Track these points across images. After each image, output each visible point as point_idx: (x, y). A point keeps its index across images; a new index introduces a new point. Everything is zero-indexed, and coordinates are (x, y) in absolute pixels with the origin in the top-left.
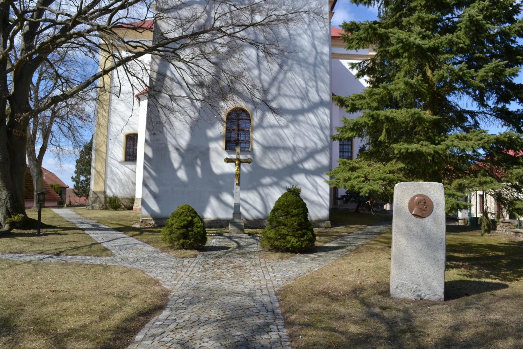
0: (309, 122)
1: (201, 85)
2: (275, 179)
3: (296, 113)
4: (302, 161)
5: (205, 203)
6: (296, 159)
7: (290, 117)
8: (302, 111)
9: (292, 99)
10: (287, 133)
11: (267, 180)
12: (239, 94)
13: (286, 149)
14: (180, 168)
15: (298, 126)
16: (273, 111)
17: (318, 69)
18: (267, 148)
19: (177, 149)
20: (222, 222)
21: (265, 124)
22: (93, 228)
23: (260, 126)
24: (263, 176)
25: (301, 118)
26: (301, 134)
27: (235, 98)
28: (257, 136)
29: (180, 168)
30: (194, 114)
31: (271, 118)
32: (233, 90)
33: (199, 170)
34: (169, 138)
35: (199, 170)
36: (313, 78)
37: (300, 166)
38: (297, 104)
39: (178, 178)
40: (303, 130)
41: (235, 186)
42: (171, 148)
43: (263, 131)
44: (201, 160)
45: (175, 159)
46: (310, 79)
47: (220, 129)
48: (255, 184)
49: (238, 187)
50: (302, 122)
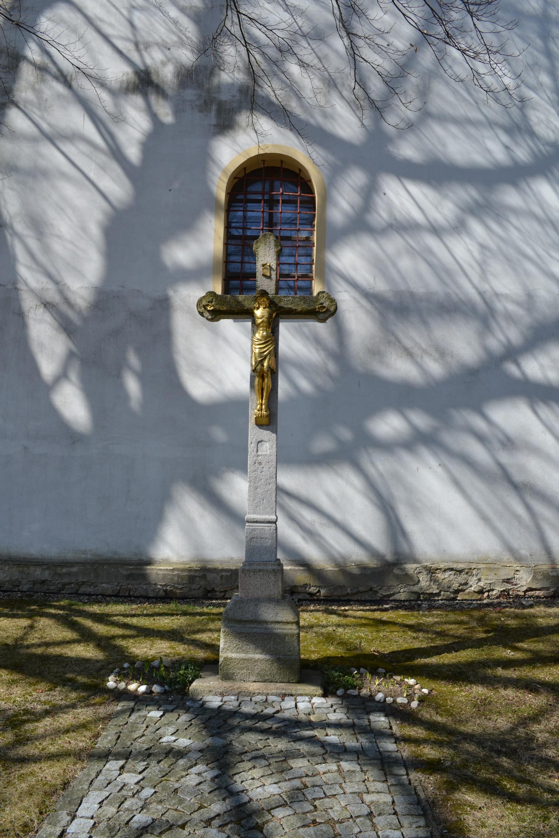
0: (537, 210)
1: (144, 82)
2: (421, 420)
3: (488, 178)
4: (512, 353)
6: (495, 343)
7: (468, 193)
8: (515, 174)
10: (461, 250)
11: (389, 425)
12: (281, 115)
14: (62, 376)
15: (500, 224)
16: (408, 171)
17: (187, 56)
18: (395, 308)
19: (47, 305)
20: (210, 576)
21: (380, 215)
23: (360, 224)
25: (511, 197)
26: (512, 252)
27: (265, 124)
28: (350, 260)
29: (62, 376)
31: (402, 198)
32: (251, 99)
33: (132, 385)
34: (28, 275)
35: (132, 385)
36: (543, 60)
37: (512, 369)
38: (493, 149)
40: (515, 235)
41: (254, 433)
42: (28, 303)
43: (369, 242)
44: (138, 351)
45: (48, 346)
46: (533, 66)
48: (346, 434)
49: (266, 434)
50: (515, 211)
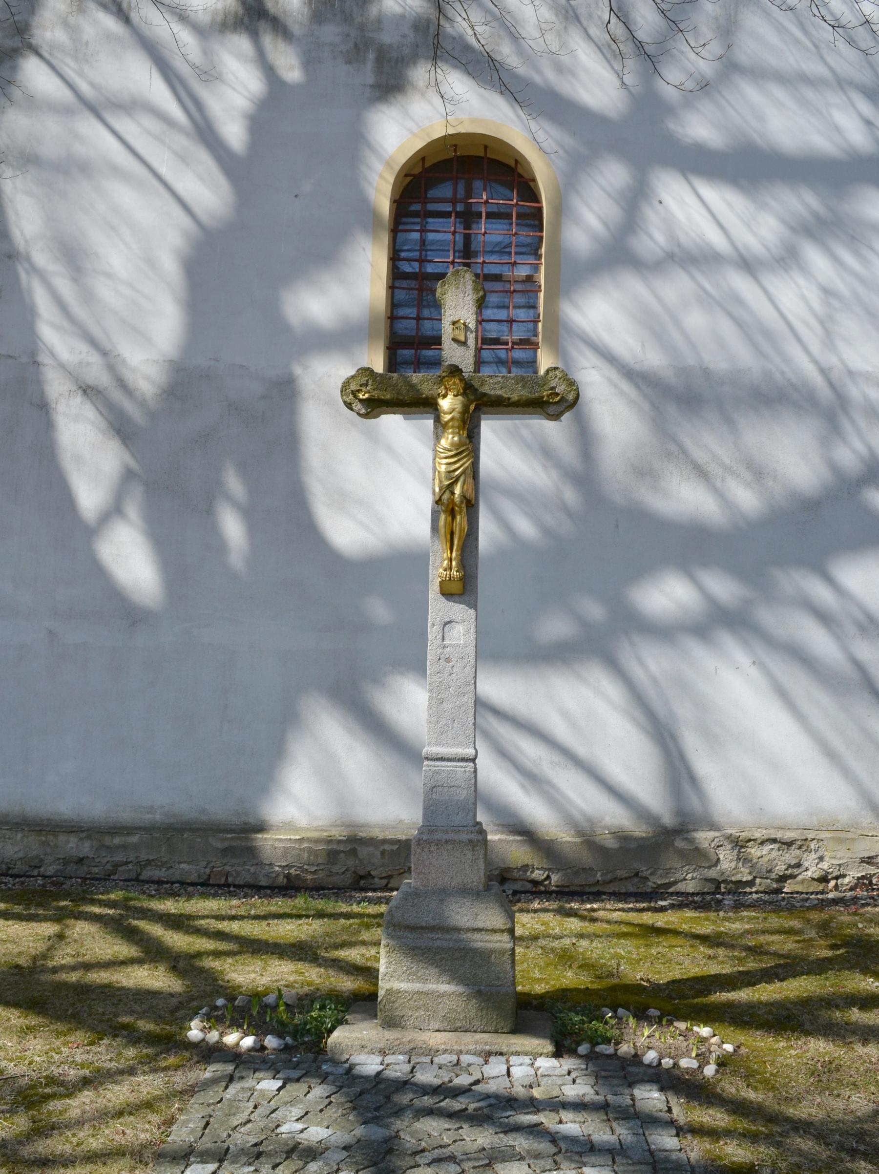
2: (723, 587)
5: (266, 762)
7: (802, 201)
9: (809, 93)
10: (791, 298)
11: (668, 595)
12: (484, 68)
13: (774, 397)
14: (114, 511)
15: (857, 254)
16: (700, 163)
21: (653, 239)
22: (751, 965)
23: (618, 254)
24: (644, 568)
27: (457, 83)
29: (114, 511)
30: (206, 190)
33: (233, 527)
34: (56, 341)
35: (233, 527)
39: (98, 572)
43: (633, 285)
44: (243, 469)
45: (90, 459)
47: (361, 280)
48: (594, 611)
